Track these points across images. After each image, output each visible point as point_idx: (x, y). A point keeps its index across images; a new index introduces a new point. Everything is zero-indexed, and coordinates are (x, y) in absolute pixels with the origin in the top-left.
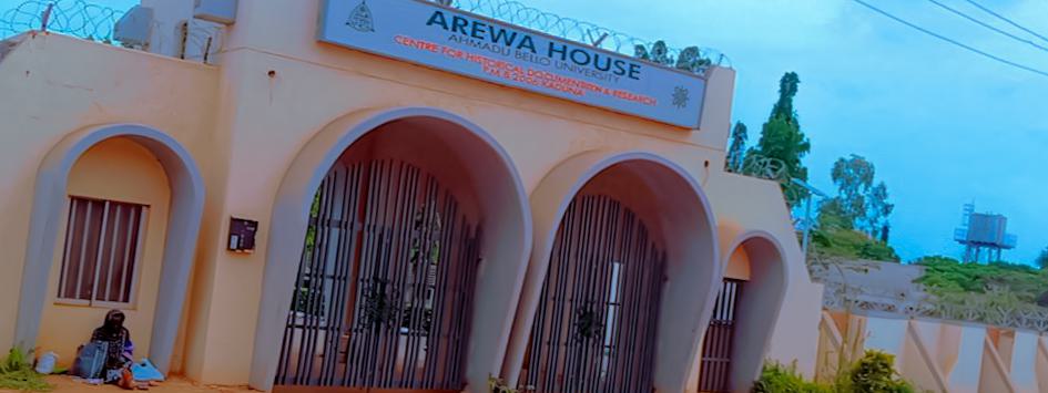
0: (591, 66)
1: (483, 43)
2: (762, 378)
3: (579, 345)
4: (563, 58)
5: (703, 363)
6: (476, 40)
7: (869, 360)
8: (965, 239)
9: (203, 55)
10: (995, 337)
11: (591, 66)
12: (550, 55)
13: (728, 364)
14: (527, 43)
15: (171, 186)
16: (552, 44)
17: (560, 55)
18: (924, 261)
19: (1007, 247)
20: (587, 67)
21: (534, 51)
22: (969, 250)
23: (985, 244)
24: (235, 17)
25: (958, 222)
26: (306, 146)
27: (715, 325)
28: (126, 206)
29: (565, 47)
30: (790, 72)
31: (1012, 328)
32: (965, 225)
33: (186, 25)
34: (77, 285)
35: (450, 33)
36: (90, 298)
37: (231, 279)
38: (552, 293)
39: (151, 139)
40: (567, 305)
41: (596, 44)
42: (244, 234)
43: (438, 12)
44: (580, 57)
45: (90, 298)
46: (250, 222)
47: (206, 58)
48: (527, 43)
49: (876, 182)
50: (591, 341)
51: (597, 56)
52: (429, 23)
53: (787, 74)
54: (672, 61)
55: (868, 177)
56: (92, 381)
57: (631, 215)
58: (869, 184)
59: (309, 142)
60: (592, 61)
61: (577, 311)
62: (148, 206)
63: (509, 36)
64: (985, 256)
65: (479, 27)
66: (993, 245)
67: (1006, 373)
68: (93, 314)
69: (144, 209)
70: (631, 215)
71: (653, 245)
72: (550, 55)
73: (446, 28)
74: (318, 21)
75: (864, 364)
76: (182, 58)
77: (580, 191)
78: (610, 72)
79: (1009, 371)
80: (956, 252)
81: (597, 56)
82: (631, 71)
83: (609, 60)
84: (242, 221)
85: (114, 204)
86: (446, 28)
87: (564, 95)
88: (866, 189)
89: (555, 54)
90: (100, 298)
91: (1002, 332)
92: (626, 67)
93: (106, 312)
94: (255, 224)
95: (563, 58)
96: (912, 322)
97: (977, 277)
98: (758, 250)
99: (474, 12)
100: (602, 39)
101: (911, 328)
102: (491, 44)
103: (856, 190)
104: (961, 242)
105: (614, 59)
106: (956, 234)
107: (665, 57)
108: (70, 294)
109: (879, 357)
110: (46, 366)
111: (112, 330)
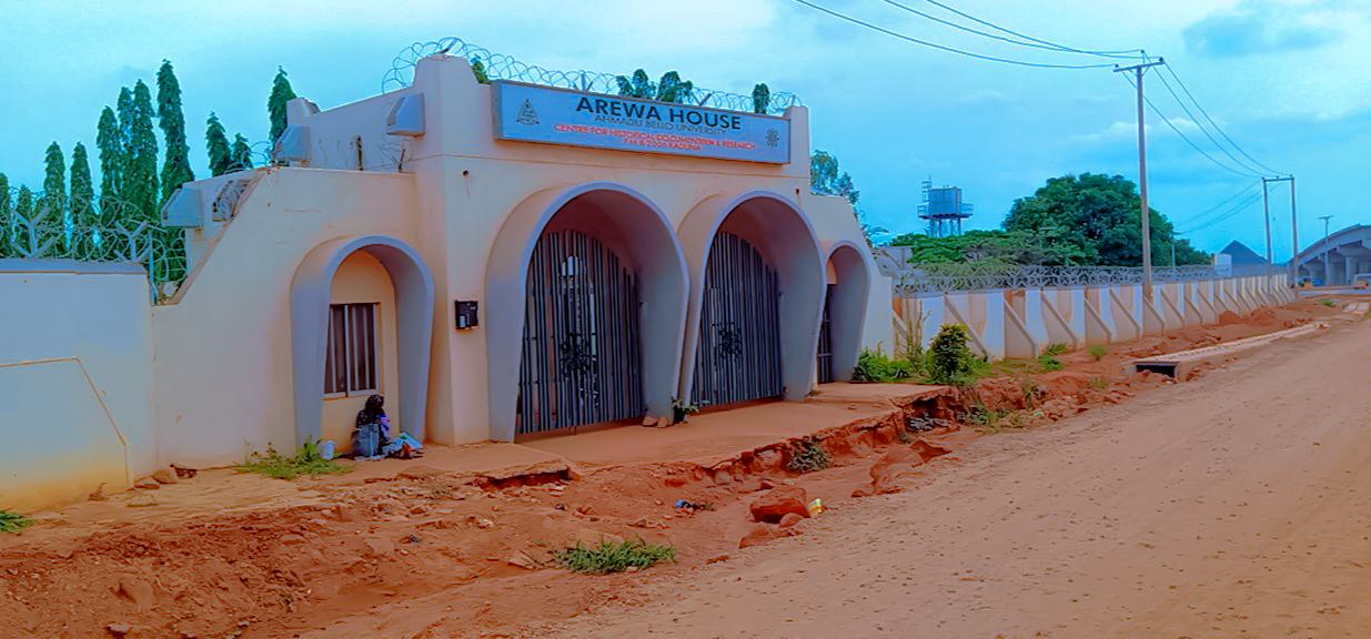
0: (703, 124)
1: (621, 118)
2: (860, 364)
3: (567, 379)
4: (682, 121)
5: (819, 359)
6: (616, 117)
7: (948, 333)
8: (927, 214)
9: (397, 165)
10: (1009, 298)
11: (703, 124)
12: (672, 120)
13: (830, 357)
14: (653, 113)
15: (395, 285)
16: (671, 110)
17: (675, 113)
18: (899, 241)
19: (965, 216)
20: (701, 125)
21: (659, 119)
22: (933, 224)
23: (947, 216)
24: (424, 129)
25: (921, 201)
26: (501, 229)
27: (822, 326)
28: (359, 306)
29: (682, 112)
30: (760, 84)
31: (1022, 289)
32: (925, 201)
33: (359, 139)
34: (337, 382)
35: (595, 114)
36: (345, 390)
37: (464, 357)
38: (533, 334)
39: (387, 246)
40: (550, 341)
41: (701, 104)
42: (467, 313)
43: (584, 98)
44: (694, 118)
45: (345, 390)
46: (471, 302)
47: (400, 168)
48: (653, 113)
49: (840, 175)
50: (734, 356)
51: (706, 115)
52: (579, 109)
53: (757, 86)
54: (654, 88)
55: (832, 172)
56: (375, 458)
57: (754, 243)
58: (835, 176)
59: (503, 227)
60: (704, 120)
61: (561, 347)
62: (377, 304)
63: (639, 109)
64: (948, 228)
65: (616, 106)
66: (953, 216)
67: (1022, 324)
68: (357, 401)
69: (375, 306)
70: (754, 243)
71: (767, 267)
72: (672, 120)
73: (591, 111)
74: (494, 122)
75: (943, 337)
76: (361, 169)
77: (719, 229)
78: (719, 126)
79: (1024, 321)
80: (920, 227)
81: (706, 115)
82: (734, 123)
83: (716, 116)
84: (465, 303)
85: (350, 306)
86: (591, 111)
87: (684, 152)
88: (832, 181)
89: (675, 118)
90: (362, 387)
91: (1013, 293)
92: (729, 120)
93: (366, 399)
94: (474, 304)
95: (682, 121)
96: (949, 297)
97: (959, 248)
98: (845, 258)
99: (609, 93)
100: (705, 100)
101: (947, 303)
102: (627, 118)
103: (823, 183)
104: (925, 218)
105: (719, 115)
106: (919, 211)
107: (646, 84)
108: (328, 390)
109: (954, 329)
110: (329, 453)
111: (373, 411)
